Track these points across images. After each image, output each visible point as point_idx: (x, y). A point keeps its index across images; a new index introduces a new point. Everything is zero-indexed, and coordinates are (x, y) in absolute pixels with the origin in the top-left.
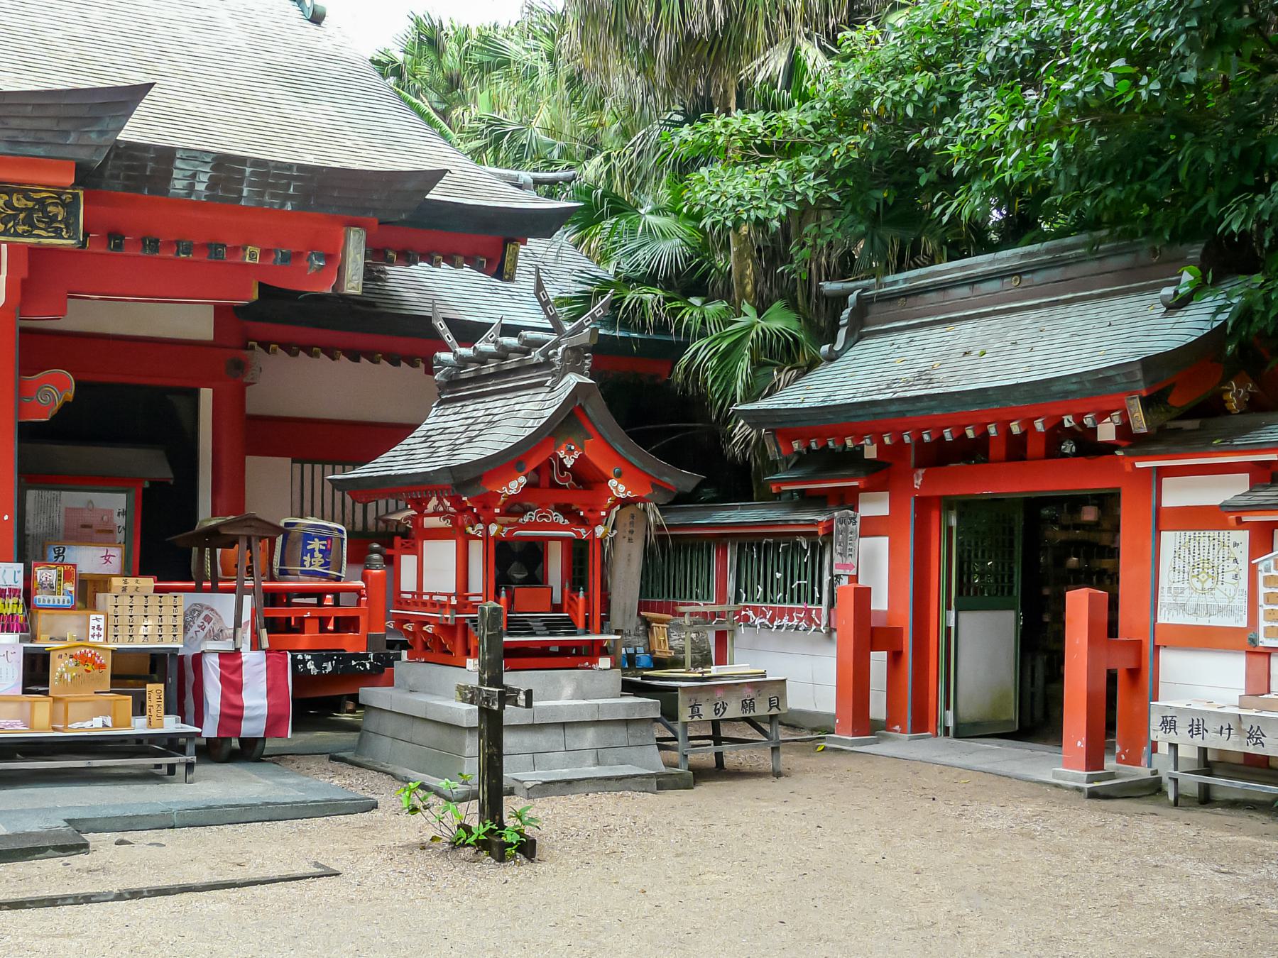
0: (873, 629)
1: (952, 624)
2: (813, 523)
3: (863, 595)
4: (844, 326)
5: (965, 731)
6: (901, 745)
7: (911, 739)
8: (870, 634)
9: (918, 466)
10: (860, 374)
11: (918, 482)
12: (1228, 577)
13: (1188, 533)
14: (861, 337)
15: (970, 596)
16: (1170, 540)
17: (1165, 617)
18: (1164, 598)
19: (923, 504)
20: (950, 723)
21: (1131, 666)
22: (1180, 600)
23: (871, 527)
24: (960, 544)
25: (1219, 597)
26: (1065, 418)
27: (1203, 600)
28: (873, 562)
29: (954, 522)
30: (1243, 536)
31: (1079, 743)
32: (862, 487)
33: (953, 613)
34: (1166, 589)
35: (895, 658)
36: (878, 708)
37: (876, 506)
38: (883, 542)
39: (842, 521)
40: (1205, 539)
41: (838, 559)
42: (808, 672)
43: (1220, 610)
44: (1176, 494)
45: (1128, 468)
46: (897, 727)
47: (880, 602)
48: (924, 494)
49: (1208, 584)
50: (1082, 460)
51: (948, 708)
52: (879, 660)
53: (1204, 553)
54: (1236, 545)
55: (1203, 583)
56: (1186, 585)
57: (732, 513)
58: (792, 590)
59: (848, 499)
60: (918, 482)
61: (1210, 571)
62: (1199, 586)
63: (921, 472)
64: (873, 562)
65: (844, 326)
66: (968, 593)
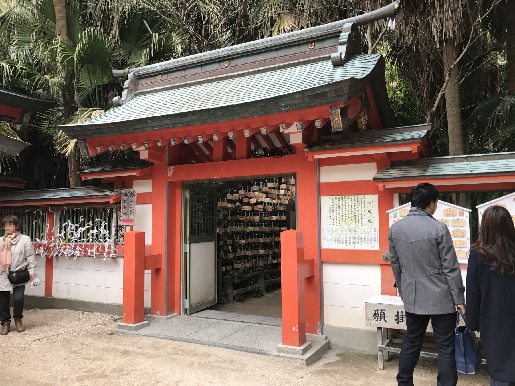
0: (145, 257)
1: (188, 251)
2: (107, 197)
3: (141, 237)
4: (126, 88)
5: (195, 309)
6: (163, 325)
7: (167, 319)
8: (143, 260)
9: (170, 164)
10: (146, 103)
11: (170, 173)
12: (365, 221)
13: (338, 197)
14: (136, 95)
15: (197, 235)
16: (326, 201)
17: (326, 245)
18: (325, 234)
19: (172, 186)
20: (187, 307)
21: (308, 276)
22: (335, 235)
23: (143, 199)
24: (191, 208)
25: (361, 232)
26: (280, 126)
27: (350, 235)
28: (144, 219)
29: (188, 196)
30: (374, 198)
31: (294, 328)
32: (138, 175)
33: (188, 245)
34: (325, 229)
35: (157, 272)
36: (148, 303)
37: (144, 187)
38: (149, 208)
39: (126, 195)
40: (349, 201)
41: (124, 217)
42: (103, 281)
43: (361, 240)
44: (329, 176)
45: (310, 159)
46: (158, 312)
47: (148, 241)
48: (173, 180)
49: (353, 225)
50: (269, 159)
51: (186, 298)
52: (148, 274)
53: (349, 208)
54: (369, 203)
55: (349, 225)
56: (338, 226)
57: (59, 193)
58: (32, 225)
59: (126, 183)
60: (170, 173)
61: (353, 218)
62: (347, 227)
63: (172, 167)
64: (144, 219)
65: (126, 88)
66: (195, 234)
